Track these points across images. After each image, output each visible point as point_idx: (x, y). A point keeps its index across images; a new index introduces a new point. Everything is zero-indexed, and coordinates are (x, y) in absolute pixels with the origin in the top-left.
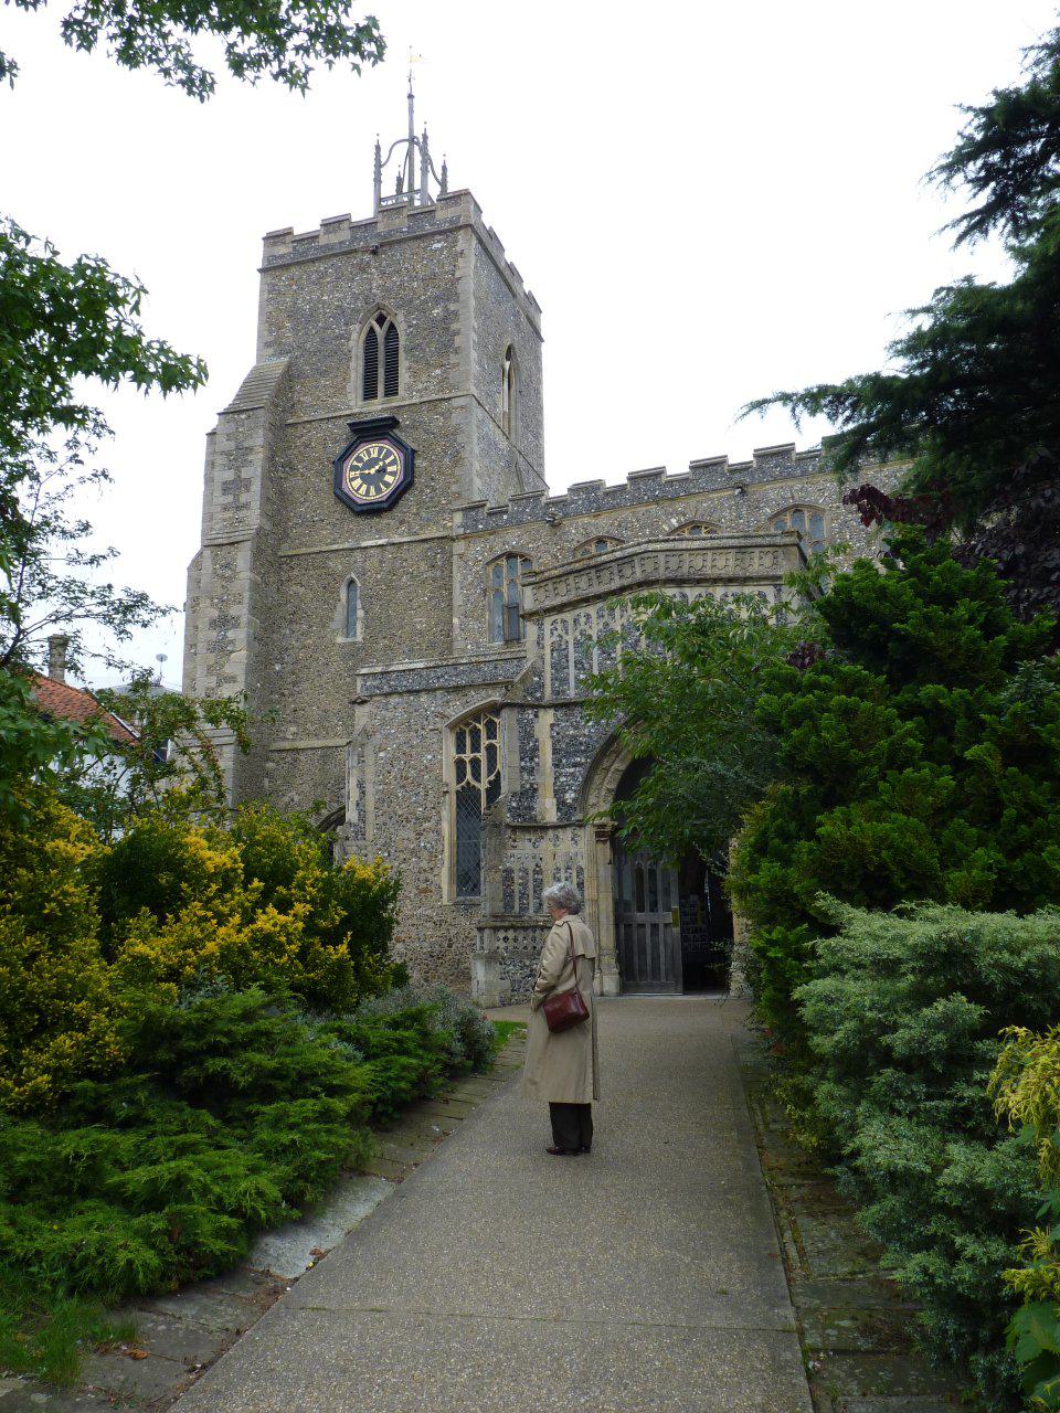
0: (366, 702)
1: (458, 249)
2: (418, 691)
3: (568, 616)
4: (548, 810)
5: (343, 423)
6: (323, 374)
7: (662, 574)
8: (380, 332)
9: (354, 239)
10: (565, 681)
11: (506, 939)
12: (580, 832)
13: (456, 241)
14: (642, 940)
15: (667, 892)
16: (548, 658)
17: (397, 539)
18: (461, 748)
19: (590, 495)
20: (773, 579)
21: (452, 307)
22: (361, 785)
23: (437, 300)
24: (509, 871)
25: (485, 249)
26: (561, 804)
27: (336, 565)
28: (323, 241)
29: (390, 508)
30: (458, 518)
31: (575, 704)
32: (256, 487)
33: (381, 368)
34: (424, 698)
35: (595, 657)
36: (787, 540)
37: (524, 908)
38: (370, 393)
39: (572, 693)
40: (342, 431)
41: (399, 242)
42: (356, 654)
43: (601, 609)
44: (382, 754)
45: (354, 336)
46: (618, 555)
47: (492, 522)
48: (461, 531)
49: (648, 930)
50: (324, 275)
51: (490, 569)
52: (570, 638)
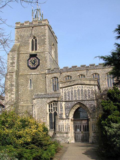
0: (35, 99)
1: (46, 28)
2: (43, 98)
3: (66, 88)
4: (64, 116)
5: (29, 54)
6: (25, 46)
7: (80, 83)
8: (34, 40)
9: (30, 25)
10: (66, 98)
11: (59, 135)
12: (69, 120)
13: (45, 27)
14: (77, 135)
15: (90, 124)
16: (64, 94)
17: (37, 73)
18: (49, 107)
19: (67, 69)
20: (94, 85)
21: (45, 37)
22: (35, 112)
23: (43, 36)
24: (59, 125)
25: (49, 29)
26: (66, 116)
27: (28, 77)
28: (25, 25)
29: (36, 68)
30: (47, 71)
31: (68, 101)
32: (16, 63)
33: (34, 47)
34: (44, 99)
35: (70, 94)
36: (96, 80)
37: (61, 131)
38: (33, 50)
39: (67, 100)
40: (28, 55)
41: (37, 26)
42: (31, 91)
43: (71, 88)
44: (38, 107)
45: (30, 40)
46: (73, 80)
47: (52, 72)
48: (47, 73)
49: (78, 134)
50: (25, 30)
51: (52, 79)
52: (67, 92)
